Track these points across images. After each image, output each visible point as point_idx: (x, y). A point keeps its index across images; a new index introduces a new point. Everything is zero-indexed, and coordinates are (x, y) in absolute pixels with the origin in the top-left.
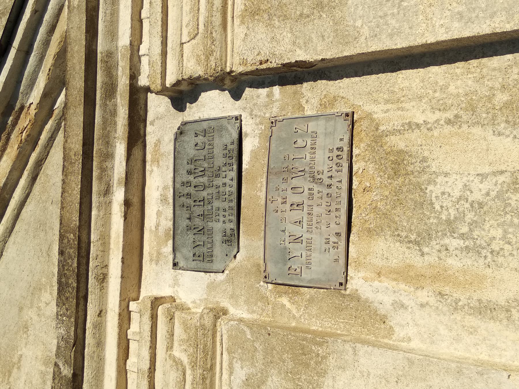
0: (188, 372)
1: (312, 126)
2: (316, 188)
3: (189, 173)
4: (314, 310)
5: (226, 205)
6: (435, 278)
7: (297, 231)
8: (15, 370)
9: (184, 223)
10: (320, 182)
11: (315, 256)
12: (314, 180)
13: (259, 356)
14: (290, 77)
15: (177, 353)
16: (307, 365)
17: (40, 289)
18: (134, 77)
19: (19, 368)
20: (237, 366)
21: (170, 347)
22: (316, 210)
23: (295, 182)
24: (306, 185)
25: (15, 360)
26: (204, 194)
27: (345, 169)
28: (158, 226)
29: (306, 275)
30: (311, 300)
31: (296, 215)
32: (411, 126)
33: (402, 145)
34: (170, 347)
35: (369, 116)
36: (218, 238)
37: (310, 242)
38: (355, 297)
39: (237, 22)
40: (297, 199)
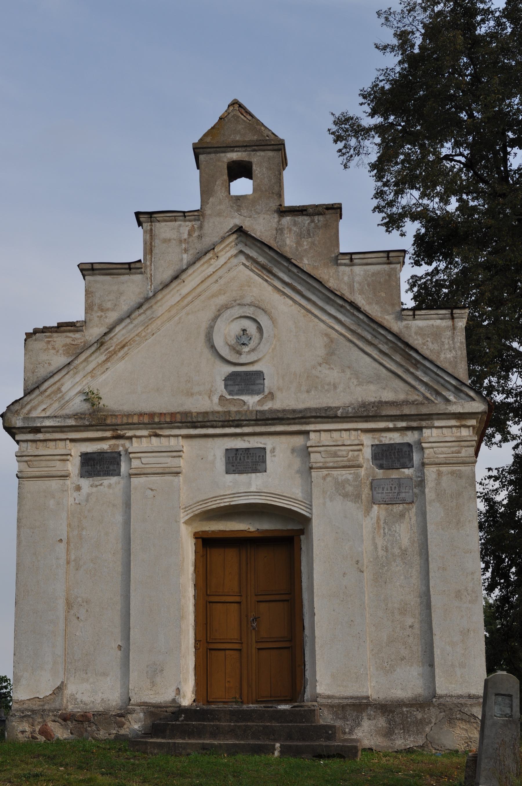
0: (346, 458)
1: (411, 491)
2: (396, 494)
3: (398, 449)
4: (367, 496)
5: (390, 465)
6: (378, 527)
7: (385, 489)
8: (328, 366)
9: (384, 448)
10: (398, 495)
11: (380, 495)
12: (398, 493)
13: (355, 483)
14: (393, 86)
15: (350, 453)
16: (356, 498)
17: (357, 379)
18: (426, 427)
19: (329, 368)
20: (351, 476)
21: (352, 451)
22: (391, 494)
23: (397, 487)
24: (396, 491)
25: (332, 366)
26: (393, 456)
27: (400, 502)
28: (383, 437)
29: (375, 493)
30: (369, 494)
31: (389, 489)
32: (410, 519)
33: (406, 517)
34: (352, 451)
35: (413, 507)
36: (381, 462)
37: (382, 493)
38: (372, 507)
39: (437, 468)
40: (393, 488)
